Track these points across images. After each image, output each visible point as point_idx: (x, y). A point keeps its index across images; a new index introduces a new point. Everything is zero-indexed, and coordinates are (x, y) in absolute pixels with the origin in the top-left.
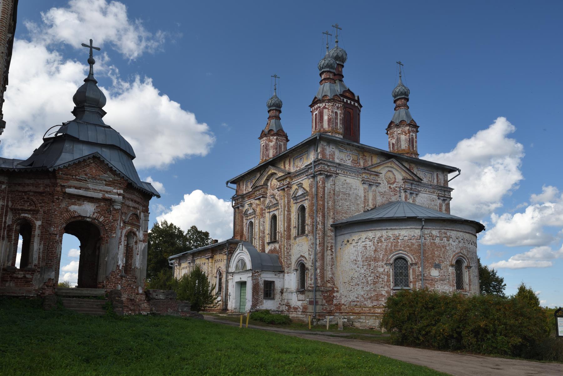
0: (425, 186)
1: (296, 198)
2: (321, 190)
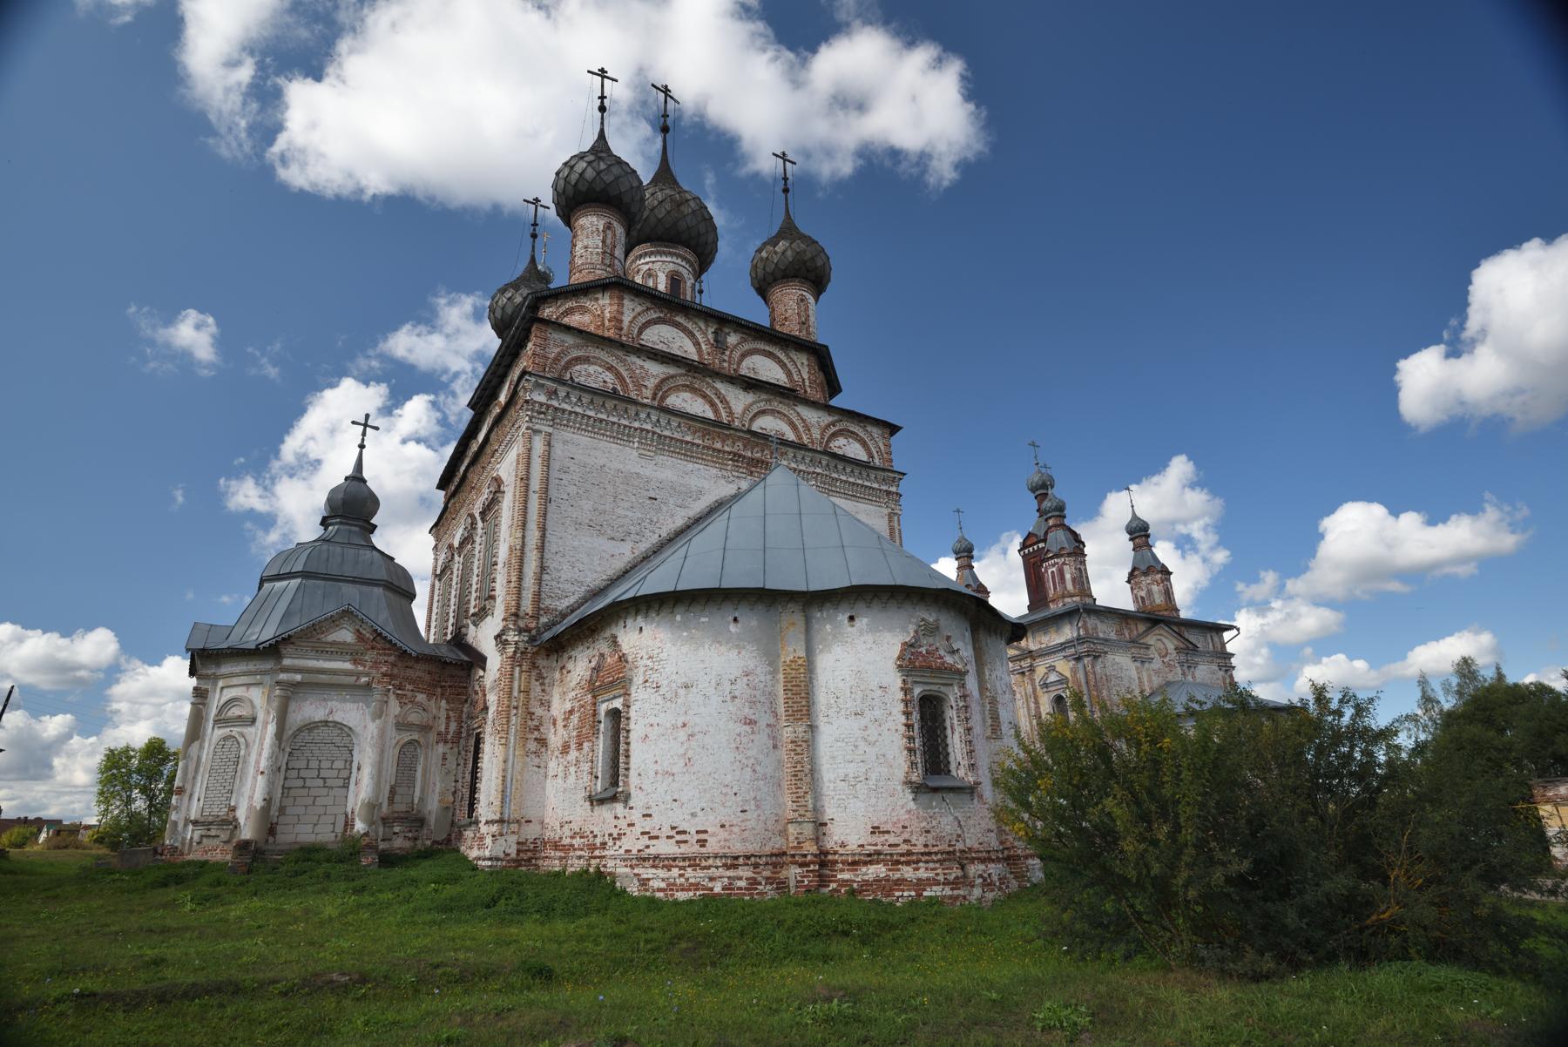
0: (1203, 654)
1: (1045, 685)
2: (1091, 676)
